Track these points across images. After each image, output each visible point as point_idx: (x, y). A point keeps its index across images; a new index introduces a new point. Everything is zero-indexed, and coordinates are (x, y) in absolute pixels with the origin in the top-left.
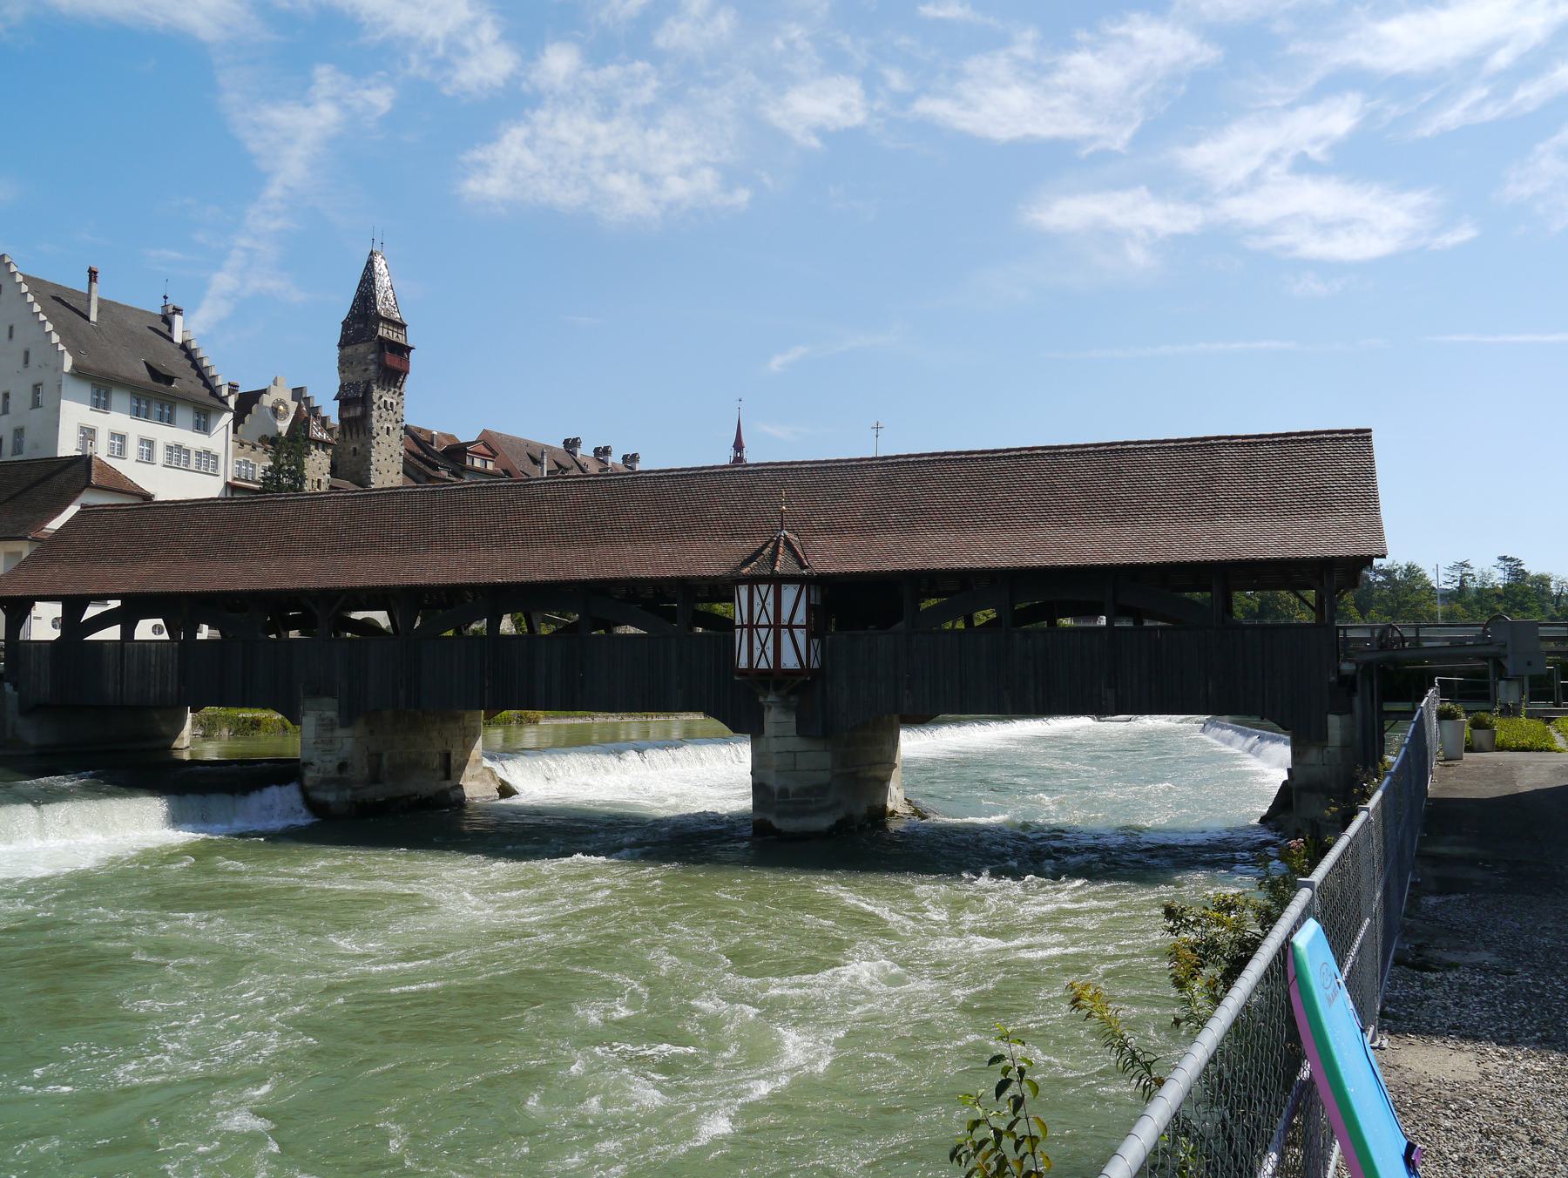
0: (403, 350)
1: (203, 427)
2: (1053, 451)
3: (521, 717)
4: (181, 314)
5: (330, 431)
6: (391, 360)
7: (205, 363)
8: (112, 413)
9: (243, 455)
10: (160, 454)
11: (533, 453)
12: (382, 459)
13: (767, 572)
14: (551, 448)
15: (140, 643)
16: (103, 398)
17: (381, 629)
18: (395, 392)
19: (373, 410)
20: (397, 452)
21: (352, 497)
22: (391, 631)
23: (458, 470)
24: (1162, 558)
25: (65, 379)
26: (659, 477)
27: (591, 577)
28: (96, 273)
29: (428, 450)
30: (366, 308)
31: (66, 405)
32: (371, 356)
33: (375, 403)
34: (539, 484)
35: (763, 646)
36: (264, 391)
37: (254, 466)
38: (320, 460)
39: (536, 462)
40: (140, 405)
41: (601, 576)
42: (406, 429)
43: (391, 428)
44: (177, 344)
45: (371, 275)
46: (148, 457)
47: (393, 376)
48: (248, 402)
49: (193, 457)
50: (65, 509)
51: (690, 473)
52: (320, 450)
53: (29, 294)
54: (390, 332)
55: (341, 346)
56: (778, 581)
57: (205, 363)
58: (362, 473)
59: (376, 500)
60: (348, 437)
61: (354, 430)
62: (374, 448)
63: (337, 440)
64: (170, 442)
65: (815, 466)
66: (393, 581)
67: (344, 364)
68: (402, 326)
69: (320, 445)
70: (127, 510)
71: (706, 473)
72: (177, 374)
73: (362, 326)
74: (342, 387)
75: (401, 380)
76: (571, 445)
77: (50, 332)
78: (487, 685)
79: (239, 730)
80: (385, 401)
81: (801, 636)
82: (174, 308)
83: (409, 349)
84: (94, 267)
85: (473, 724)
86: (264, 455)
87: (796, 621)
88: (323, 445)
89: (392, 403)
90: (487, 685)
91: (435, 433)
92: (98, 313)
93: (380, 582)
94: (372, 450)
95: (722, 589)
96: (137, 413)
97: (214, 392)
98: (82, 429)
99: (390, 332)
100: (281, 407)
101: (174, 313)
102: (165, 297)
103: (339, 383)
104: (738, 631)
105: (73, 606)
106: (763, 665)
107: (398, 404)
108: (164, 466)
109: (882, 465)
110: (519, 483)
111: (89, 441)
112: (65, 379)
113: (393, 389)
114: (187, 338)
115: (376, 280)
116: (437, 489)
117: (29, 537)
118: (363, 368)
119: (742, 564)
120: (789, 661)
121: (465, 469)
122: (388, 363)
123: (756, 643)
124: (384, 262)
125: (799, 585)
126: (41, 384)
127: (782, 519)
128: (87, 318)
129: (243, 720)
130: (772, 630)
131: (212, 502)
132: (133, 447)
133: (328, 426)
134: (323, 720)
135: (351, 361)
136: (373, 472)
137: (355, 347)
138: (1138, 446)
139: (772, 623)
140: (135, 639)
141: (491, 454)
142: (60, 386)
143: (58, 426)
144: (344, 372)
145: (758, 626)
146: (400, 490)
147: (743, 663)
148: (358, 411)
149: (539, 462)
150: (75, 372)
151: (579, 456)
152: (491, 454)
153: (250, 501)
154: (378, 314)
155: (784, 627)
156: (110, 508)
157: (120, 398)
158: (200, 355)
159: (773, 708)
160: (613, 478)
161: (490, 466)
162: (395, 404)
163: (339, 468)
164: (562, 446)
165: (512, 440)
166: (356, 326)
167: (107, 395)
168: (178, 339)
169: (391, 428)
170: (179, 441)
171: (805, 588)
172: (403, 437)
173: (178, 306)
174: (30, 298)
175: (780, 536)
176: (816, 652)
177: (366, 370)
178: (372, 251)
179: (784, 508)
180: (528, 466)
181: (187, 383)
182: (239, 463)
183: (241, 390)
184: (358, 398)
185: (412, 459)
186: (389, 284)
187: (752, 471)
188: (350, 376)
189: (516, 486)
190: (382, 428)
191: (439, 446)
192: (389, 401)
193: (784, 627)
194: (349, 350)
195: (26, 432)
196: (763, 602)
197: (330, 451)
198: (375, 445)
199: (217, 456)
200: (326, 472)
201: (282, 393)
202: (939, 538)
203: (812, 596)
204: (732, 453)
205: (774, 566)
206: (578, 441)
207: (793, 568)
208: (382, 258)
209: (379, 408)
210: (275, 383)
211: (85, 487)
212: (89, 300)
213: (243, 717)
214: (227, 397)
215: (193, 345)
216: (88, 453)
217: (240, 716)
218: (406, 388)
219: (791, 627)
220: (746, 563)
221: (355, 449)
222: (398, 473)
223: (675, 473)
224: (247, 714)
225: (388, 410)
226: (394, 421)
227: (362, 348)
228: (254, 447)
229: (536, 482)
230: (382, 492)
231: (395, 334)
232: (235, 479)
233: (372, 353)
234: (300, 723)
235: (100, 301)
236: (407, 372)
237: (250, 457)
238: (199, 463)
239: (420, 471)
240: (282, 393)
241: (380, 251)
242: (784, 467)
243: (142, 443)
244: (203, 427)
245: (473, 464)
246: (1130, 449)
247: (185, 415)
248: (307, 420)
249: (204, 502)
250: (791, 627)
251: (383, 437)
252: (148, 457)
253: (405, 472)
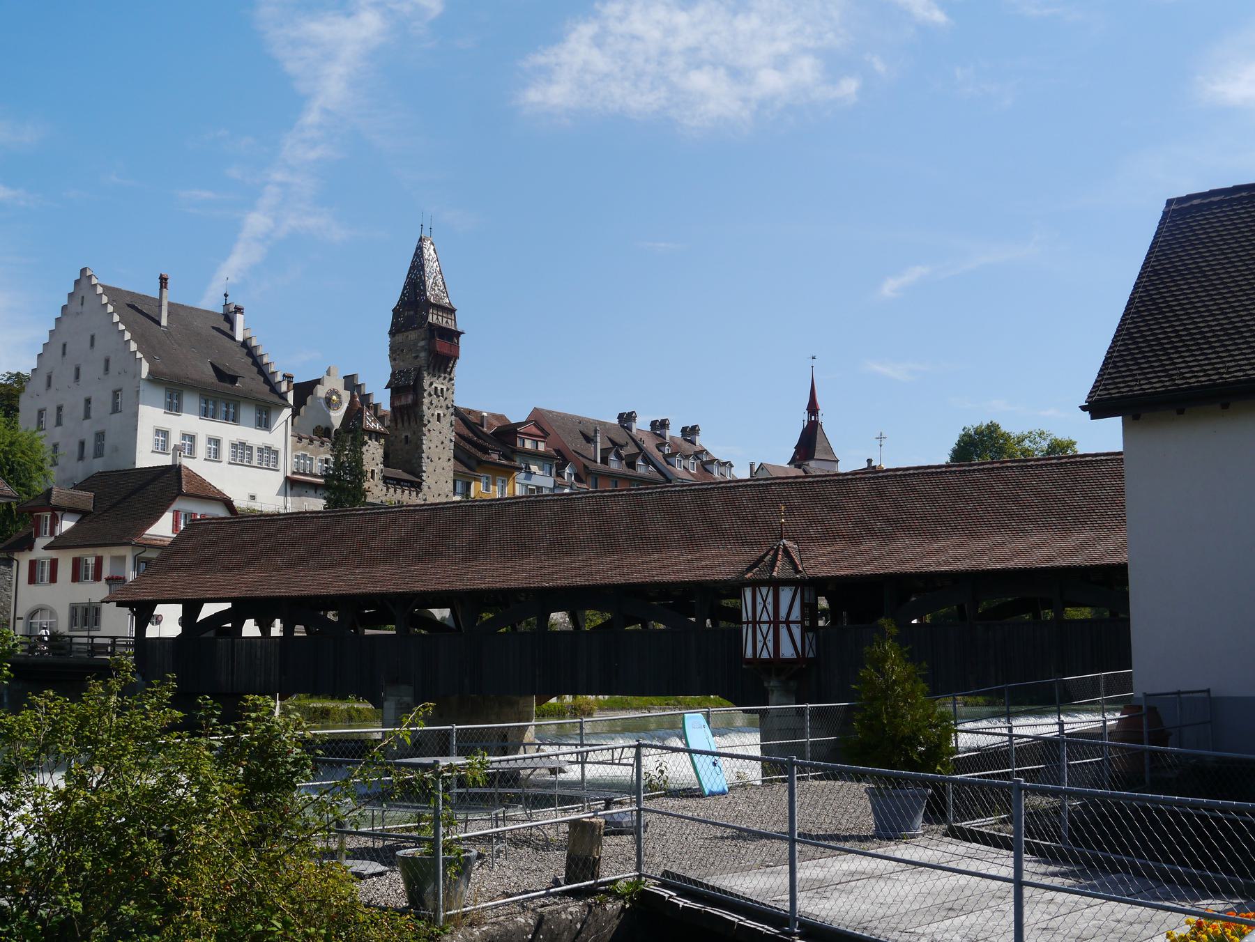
1: (264, 423)
2: (1021, 464)
3: (575, 709)
4: (242, 313)
5: (380, 419)
6: (441, 346)
7: (265, 360)
9: (301, 449)
11: (586, 431)
12: (433, 446)
14: (604, 424)
15: (248, 640)
16: (175, 401)
18: (445, 378)
19: (424, 398)
24: (1096, 561)
25: (143, 386)
26: (683, 491)
27: (623, 581)
28: (166, 279)
29: (478, 431)
30: (417, 295)
31: (143, 409)
32: (422, 343)
33: (426, 390)
36: (318, 382)
37: (311, 459)
38: (374, 451)
39: (589, 439)
40: (208, 406)
42: (457, 412)
43: (442, 415)
44: (239, 342)
45: (420, 261)
46: (215, 456)
47: (443, 362)
48: (305, 391)
49: (256, 454)
50: (161, 516)
51: (710, 487)
52: (373, 440)
53: (115, 314)
54: (440, 318)
55: (392, 333)
57: (265, 360)
60: (400, 425)
61: (405, 418)
62: (425, 435)
63: (388, 427)
65: (816, 479)
67: (395, 352)
68: (450, 311)
69: (374, 435)
71: (723, 487)
73: (412, 313)
74: (393, 375)
76: (626, 419)
77: (129, 341)
79: (310, 718)
80: (436, 388)
81: (796, 630)
82: (236, 308)
83: (458, 334)
85: (528, 709)
86: (321, 449)
88: (375, 435)
89: (442, 389)
91: (485, 414)
93: (447, 587)
94: (424, 437)
95: (734, 589)
96: (205, 414)
97: (274, 388)
99: (440, 318)
100: (334, 397)
101: (236, 312)
102: (226, 295)
103: (390, 371)
104: (745, 626)
105: (191, 609)
106: (765, 655)
107: (448, 389)
108: (230, 463)
109: (873, 478)
110: (563, 497)
111: (178, 452)
112: (143, 386)
113: (443, 375)
114: (248, 335)
115: (426, 266)
116: (493, 502)
117: (133, 543)
118: (413, 355)
119: (747, 569)
120: (787, 651)
122: (438, 350)
123: (759, 637)
124: (432, 247)
126: (120, 390)
127: (782, 531)
128: (158, 323)
129: (313, 710)
132: (202, 447)
133: (380, 414)
135: (401, 348)
136: (425, 460)
137: (406, 334)
138: (1094, 459)
141: (542, 434)
142: (138, 392)
143: (137, 430)
144: (395, 360)
146: (462, 504)
147: (749, 653)
149: (593, 440)
151: (634, 431)
152: (542, 434)
154: (427, 300)
155: (782, 622)
158: (260, 351)
159: (775, 692)
160: (643, 492)
161: (542, 447)
162: (445, 390)
163: (391, 456)
167: (179, 398)
168: (239, 337)
169: (442, 415)
170: (243, 439)
171: (799, 590)
172: (453, 423)
173: (240, 304)
174: (110, 309)
177: (417, 357)
178: (421, 237)
179: (783, 520)
181: (249, 381)
183: (295, 381)
186: (438, 269)
187: (762, 485)
188: (401, 364)
190: (433, 415)
191: (489, 428)
193: (782, 622)
194: (399, 338)
195: (106, 435)
197: (382, 441)
198: (427, 433)
199: (277, 451)
201: (335, 383)
202: (915, 544)
204: (806, 417)
205: (773, 571)
206: (634, 414)
207: (789, 573)
208: (432, 243)
210: (328, 373)
211: (178, 495)
212: (160, 306)
214: (280, 382)
216: (178, 463)
217: (311, 706)
218: (455, 374)
219: (788, 623)
220: (750, 569)
221: (406, 437)
222: (449, 460)
224: (317, 704)
225: (438, 396)
226: (444, 406)
227: (412, 335)
228: (311, 441)
229: (577, 496)
230: (446, 506)
231: (445, 320)
232: (294, 473)
233: (423, 340)
235: (170, 304)
236: (457, 357)
238: (261, 460)
239: (470, 456)
240: (335, 383)
242: (790, 480)
244: (264, 423)
246: (1088, 461)
247: (248, 413)
248: (361, 411)
250: (788, 623)
251: (434, 425)
252: (215, 456)
253: (455, 457)
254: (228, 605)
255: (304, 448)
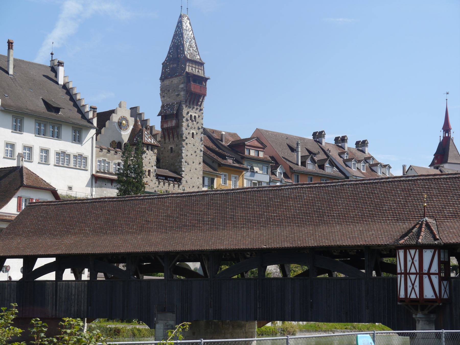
0: (202, 80)
1: (78, 139)
3: (284, 331)
4: (63, 66)
5: (154, 136)
8: (24, 133)
10: (52, 158)
11: (291, 144)
13: (414, 243)
14: (304, 139)
16: (19, 124)
17: (15, 167)
18: (197, 109)
19: (183, 122)
20: (199, 149)
21: (181, 197)
22: (201, 273)
23: (239, 158)
26: (356, 184)
27: (316, 245)
28: (12, 43)
32: (182, 86)
33: (184, 117)
34: (287, 189)
35: (413, 285)
36: (113, 111)
37: (109, 163)
40: (40, 128)
41: (321, 244)
42: (205, 132)
44: (61, 85)
45: (180, 31)
46: (45, 160)
49: (72, 159)
51: (375, 181)
52: (150, 150)
54: (194, 69)
56: (421, 248)
58: (176, 164)
59: (194, 198)
60: (167, 140)
62: (184, 147)
63: (159, 142)
64: (58, 150)
65: (448, 176)
66: (206, 247)
67: (164, 91)
68: (201, 64)
69: (150, 147)
70: (55, 205)
71: (384, 182)
72: (61, 105)
73: (175, 65)
74: (163, 107)
75: (201, 100)
76: (318, 136)
78: (258, 306)
80: (191, 116)
81: (435, 279)
82: (59, 62)
83: (206, 79)
84: (11, 39)
85: (251, 330)
87: (432, 271)
88: (151, 147)
89: (195, 117)
90: (258, 306)
91: (224, 133)
92: (14, 68)
94: (183, 148)
96: (39, 133)
97: (84, 116)
98: (7, 144)
99: (194, 69)
100: (124, 122)
101: (58, 65)
102: (52, 54)
103: (160, 104)
104: (399, 276)
106: (413, 296)
107: (199, 117)
108: (55, 165)
110: (275, 188)
111: (21, 158)
113: (196, 107)
114: (67, 81)
115: (184, 34)
118: (176, 94)
120: (429, 294)
121: (243, 158)
122: (192, 90)
123: (409, 284)
125: (433, 250)
128: (7, 72)
129: (109, 329)
130: (418, 276)
131: (102, 200)
133: (154, 133)
134: (167, 326)
136: (184, 164)
137: (171, 80)
139: (418, 272)
140: (63, 280)
141: (261, 146)
144: (164, 97)
145: (410, 274)
147: (402, 295)
148: (174, 123)
149: (296, 150)
150: (3, 109)
151: (323, 144)
152: (261, 146)
153: (123, 199)
154: (185, 57)
155: (425, 274)
156: (45, 204)
157: (29, 124)
159: (421, 322)
161: (261, 155)
163: (161, 161)
164: (311, 138)
165: (276, 135)
166: (171, 66)
167: (21, 122)
168: (61, 82)
169: (195, 133)
172: (203, 139)
173: (61, 60)
175: (423, 221)
176: (445, 288)
177: (178, 95)
179: (426, 204)
180: (287, 153)
182: (100, 161)
183: (98, 111)
184: (173, 114)
185: (209, 152)
186: (192, 36)
187: (411, 180)
188: (168, 99)
189: (274, 190)
190: (189, 133)
191: (226, 142)
192: (193, 115)
193: (425, 274)
194: (167, 82)
196: (413, 259)
197: (156, 151)
198: (185, 145)
200: (153, 165)
201: (124, 112)
203: (442, 256)
205: (418, 238)
206: (323, 133)
207: (430, 241)
208: (188, 19)
209: (187, 120)
210: (120, 106)
211: (20, 186)
212: (8, 61)
213: (110, 328)
215: (71, 86)
217: (108, 326)
218: (204, 106)
219: (429, 274)
220: (402, 237)
221: (172, 148)
222: (200, 163)
223: (366, 182)
224: (112, 325)
225: (193, 121)
226: (197, 128)
227: (175, 80)
228: (109, 151)
229: (285, 188)
232: (97, 172)
233: (182, 83)
234: (155, 328)
235: (15, 60)
236: (205, 95)
237: (107, 157)
238: (75, 163)
239: (214, 161)
240: (124, 112)
241: (186, 14)
242: (430, 177)
243: (42, 152)
244: (78, 139)
245: (249, 154)
247: (67, 132)
248: (141, 131)
249: (97, 200)
252: (45, 160)
253: (204, 162)
254: (53, 259)
255: (104, 156)
